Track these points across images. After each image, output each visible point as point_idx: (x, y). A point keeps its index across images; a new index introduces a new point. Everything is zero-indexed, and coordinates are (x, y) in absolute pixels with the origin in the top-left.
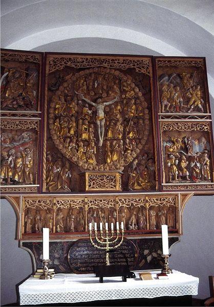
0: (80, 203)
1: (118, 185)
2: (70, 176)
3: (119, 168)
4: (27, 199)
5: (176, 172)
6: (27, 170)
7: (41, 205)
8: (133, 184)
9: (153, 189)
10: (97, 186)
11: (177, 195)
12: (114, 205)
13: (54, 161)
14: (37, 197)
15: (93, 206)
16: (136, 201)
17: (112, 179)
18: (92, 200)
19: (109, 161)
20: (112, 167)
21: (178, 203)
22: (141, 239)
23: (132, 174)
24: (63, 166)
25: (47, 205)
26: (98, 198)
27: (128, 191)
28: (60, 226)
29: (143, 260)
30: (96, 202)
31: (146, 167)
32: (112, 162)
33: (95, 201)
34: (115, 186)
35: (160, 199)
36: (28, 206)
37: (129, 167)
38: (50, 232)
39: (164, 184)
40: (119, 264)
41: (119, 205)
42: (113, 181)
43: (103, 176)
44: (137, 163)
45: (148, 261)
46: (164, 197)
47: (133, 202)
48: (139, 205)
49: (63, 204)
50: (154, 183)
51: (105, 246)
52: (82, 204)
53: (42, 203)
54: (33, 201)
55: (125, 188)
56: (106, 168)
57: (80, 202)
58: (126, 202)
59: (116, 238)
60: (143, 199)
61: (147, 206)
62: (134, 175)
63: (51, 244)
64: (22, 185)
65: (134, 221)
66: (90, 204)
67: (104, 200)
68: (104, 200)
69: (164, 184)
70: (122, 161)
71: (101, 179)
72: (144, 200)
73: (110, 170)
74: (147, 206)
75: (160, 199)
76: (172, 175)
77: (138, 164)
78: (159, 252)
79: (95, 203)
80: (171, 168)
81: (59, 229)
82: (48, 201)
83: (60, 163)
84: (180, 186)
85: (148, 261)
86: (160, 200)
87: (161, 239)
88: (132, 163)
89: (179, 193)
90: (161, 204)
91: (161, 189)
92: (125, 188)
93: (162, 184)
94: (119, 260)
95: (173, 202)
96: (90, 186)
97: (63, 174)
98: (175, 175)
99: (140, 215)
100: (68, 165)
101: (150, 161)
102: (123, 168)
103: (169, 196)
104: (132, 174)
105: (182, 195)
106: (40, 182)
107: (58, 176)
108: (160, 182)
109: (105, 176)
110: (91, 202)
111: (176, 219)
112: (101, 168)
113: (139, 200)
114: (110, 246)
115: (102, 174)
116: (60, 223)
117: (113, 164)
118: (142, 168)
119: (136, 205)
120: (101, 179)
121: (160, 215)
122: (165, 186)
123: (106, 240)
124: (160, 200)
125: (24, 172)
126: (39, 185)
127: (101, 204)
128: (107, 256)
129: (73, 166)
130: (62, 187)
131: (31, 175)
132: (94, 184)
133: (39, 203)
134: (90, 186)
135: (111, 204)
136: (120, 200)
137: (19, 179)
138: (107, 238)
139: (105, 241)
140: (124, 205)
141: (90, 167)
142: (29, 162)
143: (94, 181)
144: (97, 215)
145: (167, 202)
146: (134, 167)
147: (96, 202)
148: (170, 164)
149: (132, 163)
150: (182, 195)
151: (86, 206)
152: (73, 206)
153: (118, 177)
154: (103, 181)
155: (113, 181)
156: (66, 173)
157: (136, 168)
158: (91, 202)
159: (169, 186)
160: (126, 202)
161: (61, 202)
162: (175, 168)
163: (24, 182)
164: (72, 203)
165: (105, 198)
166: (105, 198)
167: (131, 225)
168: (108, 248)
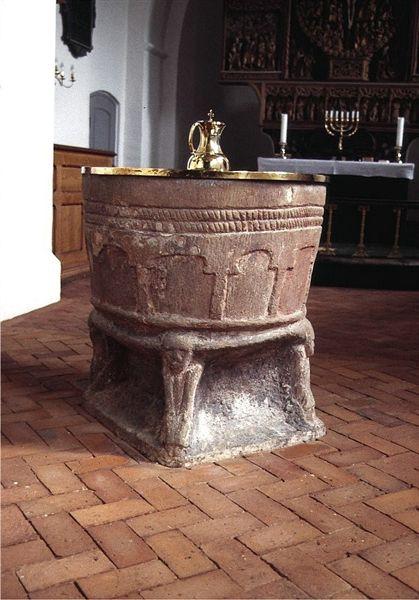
19: (356, 46)
81: (298, 117)
126: (279, 72)
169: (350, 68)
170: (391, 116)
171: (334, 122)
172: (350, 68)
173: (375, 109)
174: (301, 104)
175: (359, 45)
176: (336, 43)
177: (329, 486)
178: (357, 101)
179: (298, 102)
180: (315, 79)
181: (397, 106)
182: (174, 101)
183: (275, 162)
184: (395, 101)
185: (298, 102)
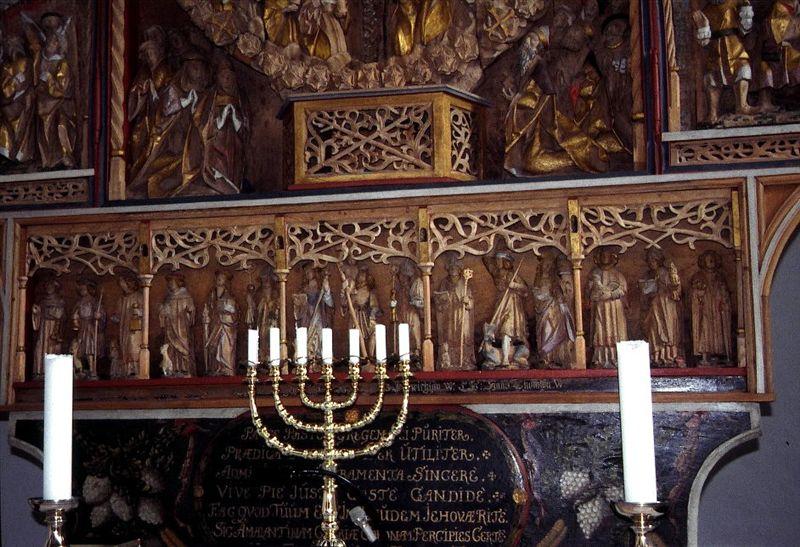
0: (255, 242)
1: (445, 150)
2: (237, 124)
3: (454, 76)
4: (35, 232)
5: (738, 67)
6: (47, 108)
7: (88, 256)
8: (526, 145)
9: (621, 164)
10: (345, 163)
11: (738, 187)
12: (412, 246)
13: (173, 65)
14: (73, 222)
15: (312, 255)
16: (518, 227)
17: (416, 125)
18: (308, 228)
19: (403, 42)
20: (415, 73)
21: (745, 231)
22: (544, 416)
23: (515, 98)
24: (209, 90)
25: (115, 254)
26: (334, 217)
27: (494, 175)
28: (174, 352)
29: (560, 523)
30: (328, 237)
31: (591, 60)
32: (419, 49)
33: (324, 229)
34: (428, 158)
35: (648, 211)
36: (39, 261)
37: (499, 68)
38: (76, 371)
39: (674, 135)
40: (434, 535)
41: (436, 245)
42: (421, 134)
43: (371, 112)
44: (544, 48)
45: (587, 531)
46: (666, 198)
47: (502, 230)
48: (535, 247)
49: (179, 249)
50: (625, 135)
51: (316, 441)
52: (265, 247)
53: (97, 250)
54: (60, 240)
55: (488, 161)
56: (389, 78)
57: (252, 237)
58: (467, 228)
59: (372, 406)
60: (552, 215)
61: (577, 247)
62: (530, 102)
63: (79, 427)
64: (24, 171)
65: (509, 325)
66: (300, 247)
67: (363, 226)
68: (363, 226)
69: (674, 135)
70: (467, 40)
71: (362, 130)
72: (559, 219)
73: (409, 83)
74: (577, 247)
75: (648, 211)
76: (722, 89)
77: (553, 52)
78: (612, 493)
79: (323, 242)
80: (712, 54)
81: (168, 365)
82: (119, 239)
83: (196, 73)
84: (761, 141)
85: (587, 531)
86: (647, 219)
87: (75, 408)
88: (519, 43)
89: (751, 174)
90: (652, 234)
91: (658, 159)
92: (489, 159)
93: (666, 137)
94: (430, 516)
95: (717, 227)
96: (312, 162)
97: (204, 119)
98: (734, 80)
99: (543, 295)
100: (225, 78)
101: (612, 28)
102: (477, 73)
103: (694, 195)
104: (515, 98)
105: (769, 187)
106: (100, 158)
107: (186, 127)
108: (655, 125)
109: (382, 112)
110: (303, 235)
111: (734, 317)
112: (365, 79)
113: (535, 220)
114: (343, 442)
115: (369, 104)
116: (176, 337)
117: (426, 55)
118: (570, 66)
119: (518, 244)
120: (362, 130)
121: (650, 297)
122: (679, 145)
123: (322, 412)
124: (647, 219)
125: (36, 121)
126: (91, 172)
127: (350, 244)
128: (329, 497)
129: (251, 86)
130: (197, 180)
131: (62, 127)
132: (329, 153)
133: (84, 250)
134: (312, 162)
135: (397, 245)
136: (440, 222)
137: (14, 150)
138: (330, 405)
139: (318, 417)
140: (461, 247)
141: (315, 79)
142: (56, 67)
143: (330, 141)
144: (335, 294)
145: (684, 223)
146: (528, 63)
147: (328, 237)
148: (706, 32)
149: (519, 43)
150: (769, 187)
151: (283, 255)
152: (225, 258)
153: (446, 114)
154: (371, 139)
155: (421, 134)
156: (219, 114)
157: (535, 73)
158: (303, 235)
159: (704, 143)
160: (467, 228)
161: (173, 241)
162: (737, 50)
163: (33, 163)
164: (219, 242)
165: (366, 216)
166: (366, 216)
167: (498, 344)
168: (332, 455)
169: (382, 131)
170: (589, 334)
171: (289, 383)
172: (382, 131)
173: (508, 305)
174: (181, 302)
175: (417, 37)
176: (320, 35)
177: (190, 313)
178: (420, 273)
179: (162, 297)
180: (249, 192)
181: (611, 287)
182: (170, 417)
183: (676, 85)
184: (602, 258)
185: (162, 297)
